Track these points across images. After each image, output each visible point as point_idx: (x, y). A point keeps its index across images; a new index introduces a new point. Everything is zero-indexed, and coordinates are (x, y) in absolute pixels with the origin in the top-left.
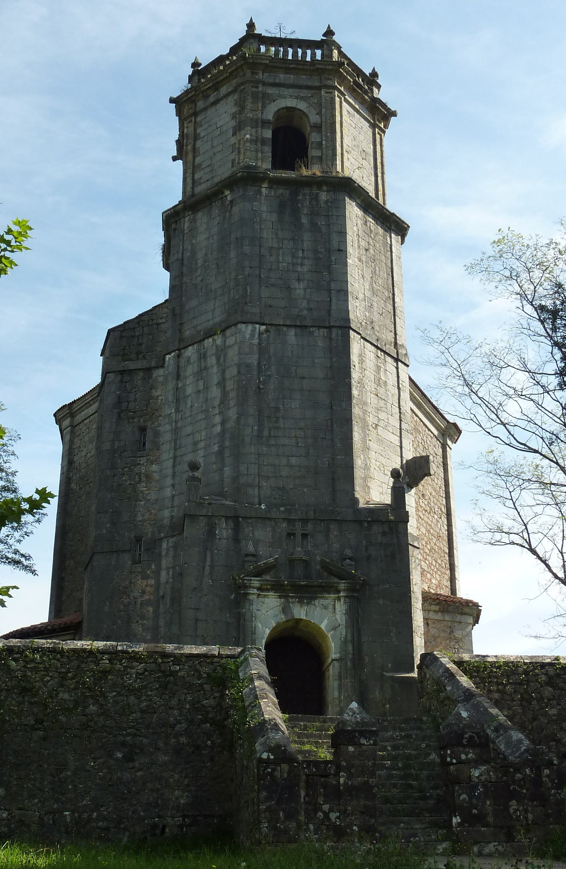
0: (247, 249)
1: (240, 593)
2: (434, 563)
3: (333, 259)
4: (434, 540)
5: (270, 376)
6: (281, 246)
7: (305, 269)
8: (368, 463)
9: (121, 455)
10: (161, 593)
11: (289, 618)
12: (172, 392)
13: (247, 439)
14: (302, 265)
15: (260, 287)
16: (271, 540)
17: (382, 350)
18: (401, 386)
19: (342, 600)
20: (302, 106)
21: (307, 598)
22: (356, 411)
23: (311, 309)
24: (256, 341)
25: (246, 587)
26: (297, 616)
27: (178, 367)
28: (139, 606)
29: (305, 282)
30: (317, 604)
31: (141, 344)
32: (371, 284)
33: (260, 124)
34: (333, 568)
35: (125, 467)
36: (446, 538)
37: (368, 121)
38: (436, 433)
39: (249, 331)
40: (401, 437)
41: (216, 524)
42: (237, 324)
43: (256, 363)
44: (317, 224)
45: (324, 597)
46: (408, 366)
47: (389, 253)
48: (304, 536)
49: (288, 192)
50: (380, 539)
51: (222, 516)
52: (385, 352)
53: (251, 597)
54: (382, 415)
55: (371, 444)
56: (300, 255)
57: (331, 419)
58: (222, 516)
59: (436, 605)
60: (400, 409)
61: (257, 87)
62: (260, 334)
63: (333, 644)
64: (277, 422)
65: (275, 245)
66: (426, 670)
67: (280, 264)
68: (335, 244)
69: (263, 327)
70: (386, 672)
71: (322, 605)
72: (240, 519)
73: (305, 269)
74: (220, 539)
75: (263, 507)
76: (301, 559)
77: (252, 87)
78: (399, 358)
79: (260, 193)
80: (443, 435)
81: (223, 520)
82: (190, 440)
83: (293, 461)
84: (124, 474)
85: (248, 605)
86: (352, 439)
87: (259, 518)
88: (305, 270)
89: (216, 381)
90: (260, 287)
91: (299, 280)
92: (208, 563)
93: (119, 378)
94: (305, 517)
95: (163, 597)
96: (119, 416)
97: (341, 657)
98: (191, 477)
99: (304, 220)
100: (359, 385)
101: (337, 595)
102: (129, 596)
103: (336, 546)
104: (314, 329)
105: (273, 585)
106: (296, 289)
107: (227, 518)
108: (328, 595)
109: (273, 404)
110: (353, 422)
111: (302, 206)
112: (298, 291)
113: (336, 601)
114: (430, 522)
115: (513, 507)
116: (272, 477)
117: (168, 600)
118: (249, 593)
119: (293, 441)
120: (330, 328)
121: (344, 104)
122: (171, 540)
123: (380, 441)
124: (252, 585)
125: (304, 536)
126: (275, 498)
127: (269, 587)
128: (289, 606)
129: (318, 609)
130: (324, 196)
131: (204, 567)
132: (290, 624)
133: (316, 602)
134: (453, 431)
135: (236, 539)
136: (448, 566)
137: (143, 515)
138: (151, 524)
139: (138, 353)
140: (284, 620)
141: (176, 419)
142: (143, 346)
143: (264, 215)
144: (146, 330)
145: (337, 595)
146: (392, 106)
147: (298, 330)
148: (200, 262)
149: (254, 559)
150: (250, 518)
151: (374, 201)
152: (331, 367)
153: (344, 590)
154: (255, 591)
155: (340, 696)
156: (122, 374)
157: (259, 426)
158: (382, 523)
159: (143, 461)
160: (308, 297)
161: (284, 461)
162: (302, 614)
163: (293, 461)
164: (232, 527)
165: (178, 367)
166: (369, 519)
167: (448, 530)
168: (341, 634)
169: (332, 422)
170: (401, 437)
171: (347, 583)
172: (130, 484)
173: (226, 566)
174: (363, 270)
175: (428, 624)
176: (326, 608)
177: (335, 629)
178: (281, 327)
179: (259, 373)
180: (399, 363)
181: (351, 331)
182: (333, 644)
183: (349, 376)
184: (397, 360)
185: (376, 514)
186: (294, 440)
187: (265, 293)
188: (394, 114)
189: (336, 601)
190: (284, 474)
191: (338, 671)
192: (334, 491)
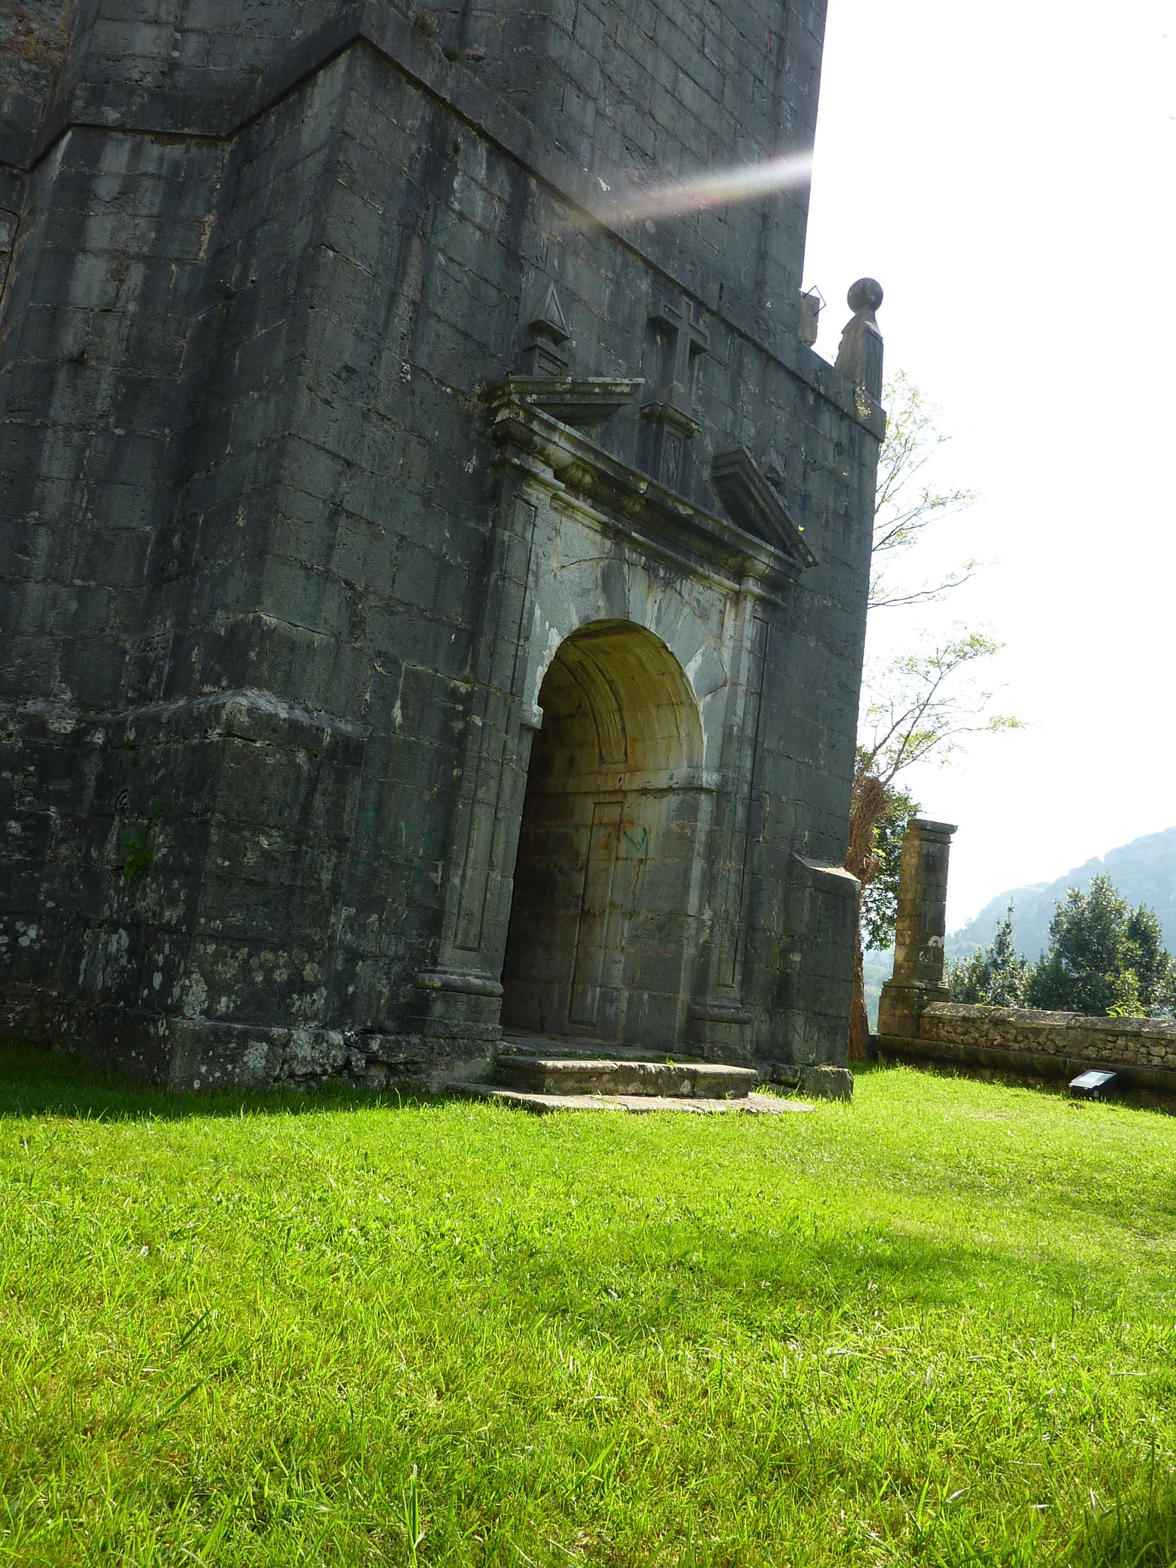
10: (69, 343)
16: (608, 318)
25: (527, 446)
41: (456, 149)
70: (798, 852)
72: (533, 183)
85: (520, 518)
92: (409, 291)
95: (78, 361)
105: (602, 475)
117: (104, 382)
122: (154, 150)
124: (551, 448)
127: (588, 479)
129: (686, 610)
131: (393, 298)
133: (686, 586)
138: (22, 72)
140: (602, 615)
154: (548, 475)
162: (649, 612)
173: (466, 335)
176: (704, 615)
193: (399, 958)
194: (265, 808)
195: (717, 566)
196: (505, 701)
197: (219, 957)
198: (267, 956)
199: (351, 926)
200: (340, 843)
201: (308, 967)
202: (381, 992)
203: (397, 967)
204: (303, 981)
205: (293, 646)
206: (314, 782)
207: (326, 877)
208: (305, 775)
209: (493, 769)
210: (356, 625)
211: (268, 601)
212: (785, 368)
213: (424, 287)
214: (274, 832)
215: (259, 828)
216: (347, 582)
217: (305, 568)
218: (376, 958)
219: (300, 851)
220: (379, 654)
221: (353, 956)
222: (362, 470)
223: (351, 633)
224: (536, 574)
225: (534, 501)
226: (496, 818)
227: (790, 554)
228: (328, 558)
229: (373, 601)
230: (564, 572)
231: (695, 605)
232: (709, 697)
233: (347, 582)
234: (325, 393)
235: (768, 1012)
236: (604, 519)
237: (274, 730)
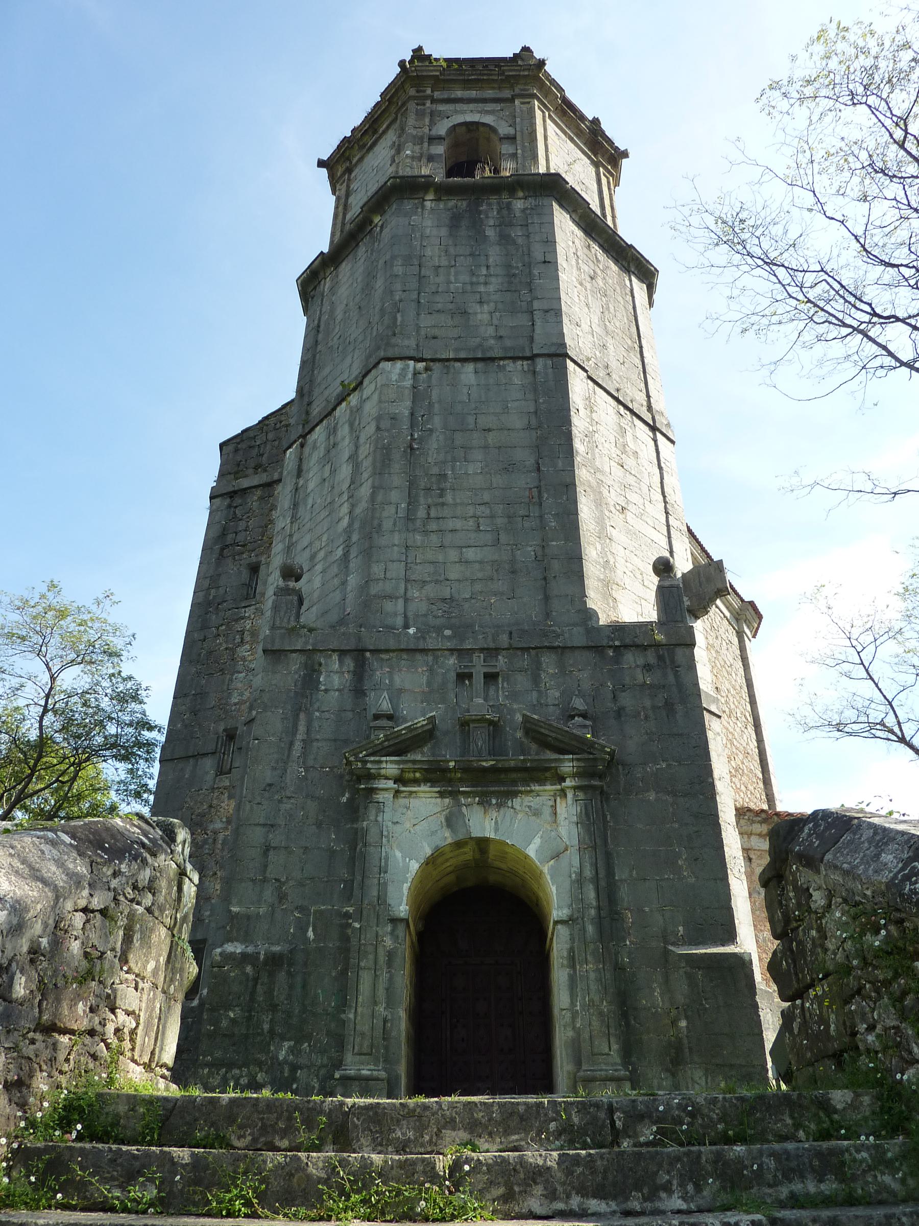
0: (399, 270)
1: (358, 790)
2: (743, 788)
3: (536, 272)
4: (741, 756)
5: (431, 430)
6: (453, 263)
7: (491, 288)
8: (612, 561)
9: (217, 608)
11: (461, 836)
12: (289, 497)
13: (387, 525)
14: (486, 283)
15: (418, 314)
17: (626, 407)
18: (663, 465)
19: (570, 795)
20: (488, 119)
21: (498, 794)
22: (582, 474)
23: (501, 337)
24: (408, 382)
25: (370, 777)
26: (476, 833)
27: (301, 459)
28: (219, 846)
29: (492, 304)
30: (518, 807)
31: (262, 455)
32: (602, 319)
33: (426, 140)
34: (546, 732)
35: (222, 625)
36: (757, 758)
37: (589, 158)
38: (728, 614)
39: (397, 371)
40: (669, 537)
41: (320, 664)
42: (378, 363)
43: (407, 413)
44: (509, 236)
45: (531, 791)
46: (673, 442)
47: (629, 298)
48: (491, 677)
49: (465, 203)
50: (640, 677)
51: (334, 651)
52: (631, 411)
53: (380, 797)
54: (633, 497)
55: (614, 533)
56: (484, 271)
57: (538, 487)
58: (334, 651)
59: (761, 823)
60: (664, 497)
61: (424, 104)
62: (416, 373)
63: (554, 889)
64: (441, 496)
65: (444, 262)
66: (804, 876)
67: (452, 286)
68: (538, 253)
69: (421, 365)
70: (673, 944)
71: (529, 807)
72: (368, 654)
73: (491, 288)
74: (326, 691)
75: (411, 631)
76: (482, 720)
77: (417, 104)
78: (658, 425)
79: (423, 207)
80: (737, 620)
81: (335, 657)
82: (307, 554)
83: (470, 554)
84: (219, 635)
86: (577, 514)
87: (402, 650)
88: (491, 290)
89: (346, 456)
90: (418, 314)
91: (481, 302)
93: (228, 501)
94: (492, 645)
96: (221, 554)
97: (572, 915)
98: (282, 589)
99: (490, 233)
100: (587, 439)
101: (559, 787)
102: (205, 829)
103: (554, 694)
104: (506, 362)
106: (476, 313)
107: (342, 653)
108: (541, 788)
109: (435, 470)
110: (578, 489)
111: (487, 217)
112: (479, 317)
113: (558, 799)
114: (731, 730)
115: (865, 675)
116: (431, 582)
118: (377, 789)
119: (471, 523)
120: (532, 358)
121: (548, 121)
123: (633, 534)
124: (383, 772)
125: (491, 677)
126: (436, 617)
127: (418, 775)
128: (460, 811)
129: (520, 816)
130: (518, 205)
131: (291, 744)
132: (468, 854)
133: (517, 802)
134: (750, 614)
135: (359, 691)
136: (764, 797)
137: (241, 694)
139: (256, 468)
140: (449, 841)
141: (291, 532)
142: (265, 455)
143: (428, 231)
144: (271, 436)
145: (559, 787)
146: (621, 145)
147: (480, 365)
148: (339, 317)
149: (390, 723)
150: (387, 651)
151: (598, 220)
152: (536, 413)
153: (574, 776)
154: (390, 784)
155: (573, 1004)
156: (231, 497)
157: (409, 504)
158: (643, 648)
159: (249, 612)
160: (495, 322)
161: (453, 555)
162: (488, 827)
163: (470, 554)
164: (352, 669)
165: (301, 459)
166: (617, 643)
167: (758, 747)
168: (571, 866)
169: (540, 492)
170: (669, 537)
171: (578, 760)
172: (226, 649)
174: (587, 297)
175: (750, 860)
176: (537, 813)
177: (557, 856)
178: (452, 363)
179: (412, 426)
180: (658, 434)
181: (568, 361)
182: (554, 889)
183: (568, 422)
184: (654, 428)
185: (626, 637)
186: (471, 522)
187: (426, 321)
188: (625, 154)
189: (558, 799)
190: (453, 576)
191: (568, 946)
192: (547, 598)
193: (323, 1066)
194: (231, 997)
195: (542, 782)
196: (375, 909)
197: (210, 1074)
198: (236, 1071)
199: (292, 1051)
200: (274, 1008)
201: (259, 1075)
202: (314, 1087)
203: (323, 1072)
204: (257, 1082)
205: (248, 917)
206: (256, 980)
207: (266, 1027)
208: (251, 977)
209: (370, 949)
210: (282, 897)
211: (234, 901)
212: (579, 647)
213: (308, 732)
214: (237, 1009)
215: (228, 1007)
216: (276, 879)
217: (252, 880)
218: (308, 1067)
219: (251, 1015)
220: (297, 908)
221: (294, 1068)
222: (280, 826)
223: (280, 902)
224: (387, 837)
225: (381, 800)
226: (376, 976)
227: (591, 753)
228: (265, 871)
229: (291, 883)
230: (416, 827)
231: (527, 809)
232: (552, 862)
233: (276, 879)
234: (258, 799)
235: (667, 1070)
236: (438, 789)
237: (234, 959)
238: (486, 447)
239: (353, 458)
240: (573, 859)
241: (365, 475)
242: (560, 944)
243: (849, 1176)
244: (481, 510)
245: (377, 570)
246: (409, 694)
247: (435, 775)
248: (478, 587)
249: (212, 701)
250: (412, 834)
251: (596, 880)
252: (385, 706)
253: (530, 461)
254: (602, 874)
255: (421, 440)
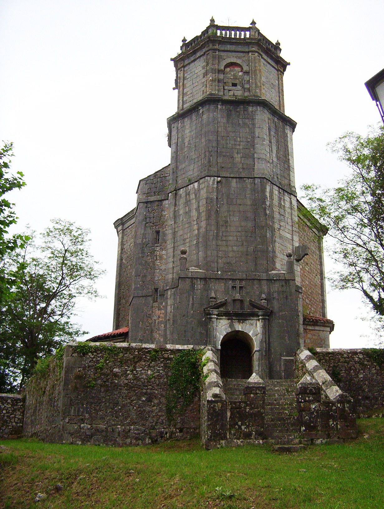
21: (242, 320)
64: (226, 228)
69: (219, 179)
75: (219, 273)
83: (235, 248)
109: (224, 219)
125: (241, 288)
147: (238, 180)
153: (261, 316)
154: (216, 316)
176: (252, 325)
186: (235, 238)
187: (220, 160)
188: (289, 64)
190: (230, 255)
192: (256, 265)
238: (239, 211)
239: (198, 209)
240: (260, 336)
241: (203, 219)
242: (256, 356)
243: (21, 183)
244: (238, 234)
245: (209, 253)
246: (219, 292)
247: (228, 315)
248: (237, 259)
249: (149, 278)
250: (222, 328)
251: (266, 342)
252: (213, 295)
253: (253, 217)
254: (267, 340)
255: (220, 208)
